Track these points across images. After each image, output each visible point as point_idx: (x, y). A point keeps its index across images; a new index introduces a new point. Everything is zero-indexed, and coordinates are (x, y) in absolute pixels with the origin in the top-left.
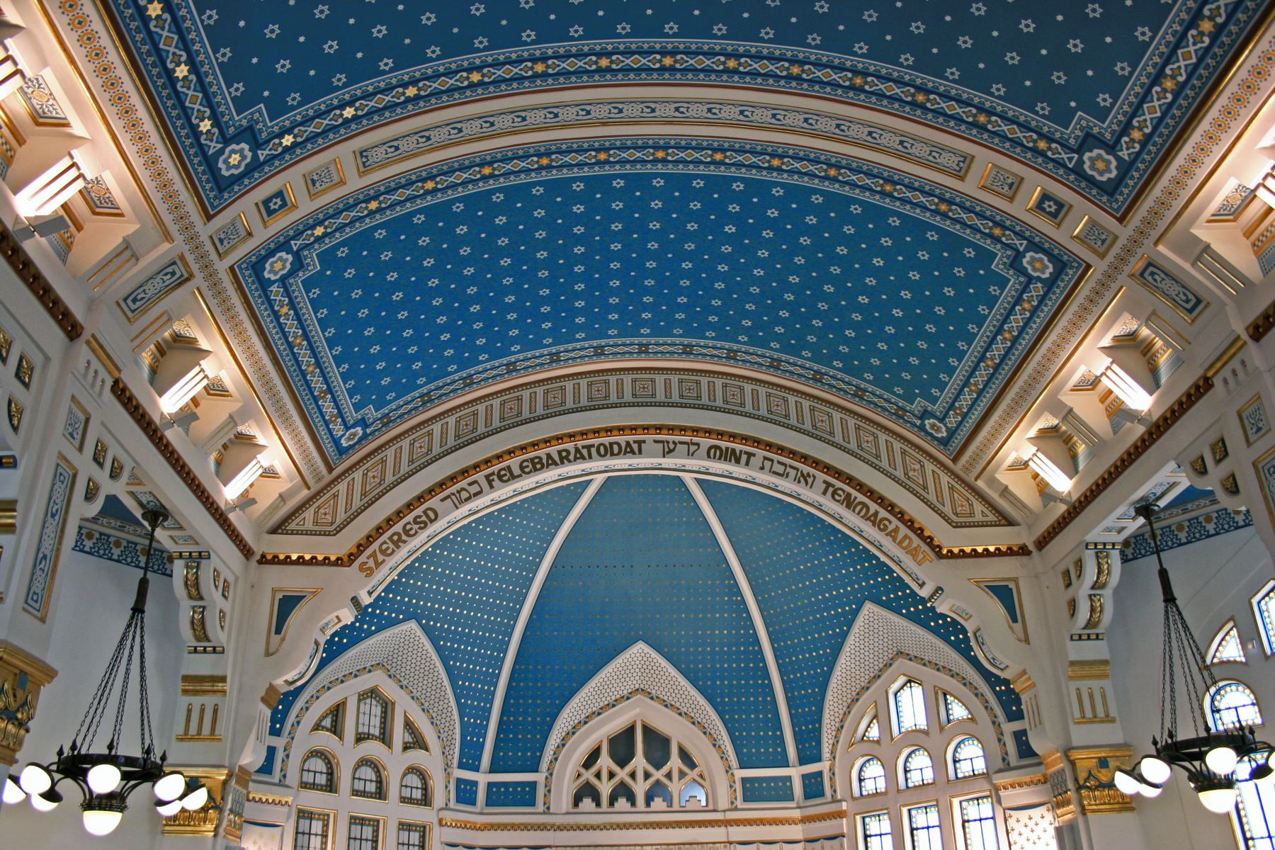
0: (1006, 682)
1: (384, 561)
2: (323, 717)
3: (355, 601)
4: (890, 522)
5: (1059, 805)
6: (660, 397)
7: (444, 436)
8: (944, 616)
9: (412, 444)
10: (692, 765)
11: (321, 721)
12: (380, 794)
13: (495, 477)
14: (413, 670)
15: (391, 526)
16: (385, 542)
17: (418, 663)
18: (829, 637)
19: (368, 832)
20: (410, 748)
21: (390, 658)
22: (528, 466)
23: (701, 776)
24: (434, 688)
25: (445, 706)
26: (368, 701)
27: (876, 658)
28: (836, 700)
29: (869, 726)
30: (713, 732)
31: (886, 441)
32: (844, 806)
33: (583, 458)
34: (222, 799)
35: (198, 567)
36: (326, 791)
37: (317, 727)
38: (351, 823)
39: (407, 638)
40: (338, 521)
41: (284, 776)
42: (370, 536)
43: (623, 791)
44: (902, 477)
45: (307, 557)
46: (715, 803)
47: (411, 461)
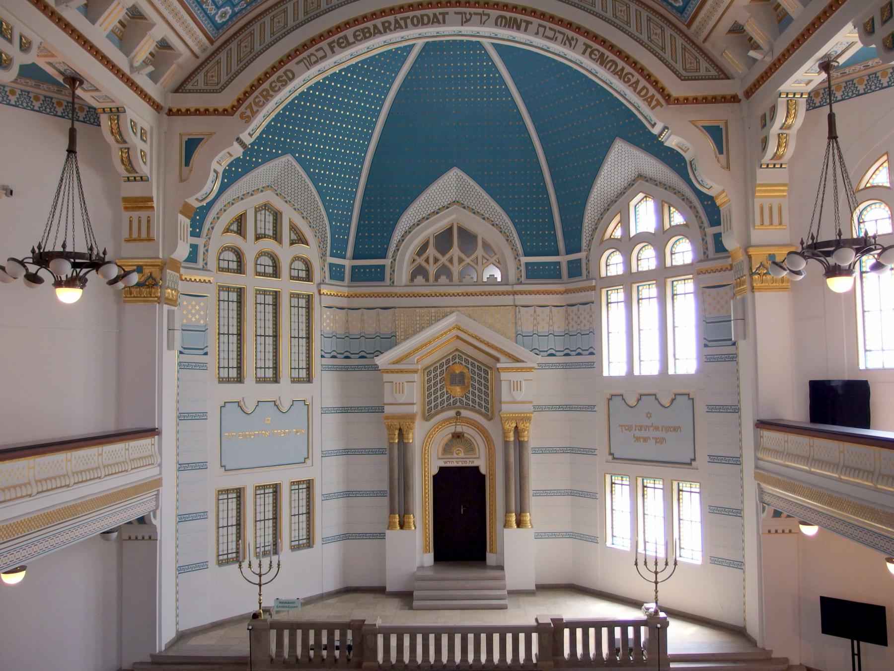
0: (711, 198)
1: (258, 111)
4: (633, 76)
9: (272, 20)
11: (229, 226)
13: (335, 44)
16: (257, 97)
17: (296, 185)
21: (276, 182)
22: (360, 35)
30: (506, 231)
31: (636, 10)
35: (118, 119)
36: (237, 273)
37: (227, 230)
38: (256, 294)
40: (223, 81)
41: (206, 264)
43: (444, 271)
47: (273, 34)
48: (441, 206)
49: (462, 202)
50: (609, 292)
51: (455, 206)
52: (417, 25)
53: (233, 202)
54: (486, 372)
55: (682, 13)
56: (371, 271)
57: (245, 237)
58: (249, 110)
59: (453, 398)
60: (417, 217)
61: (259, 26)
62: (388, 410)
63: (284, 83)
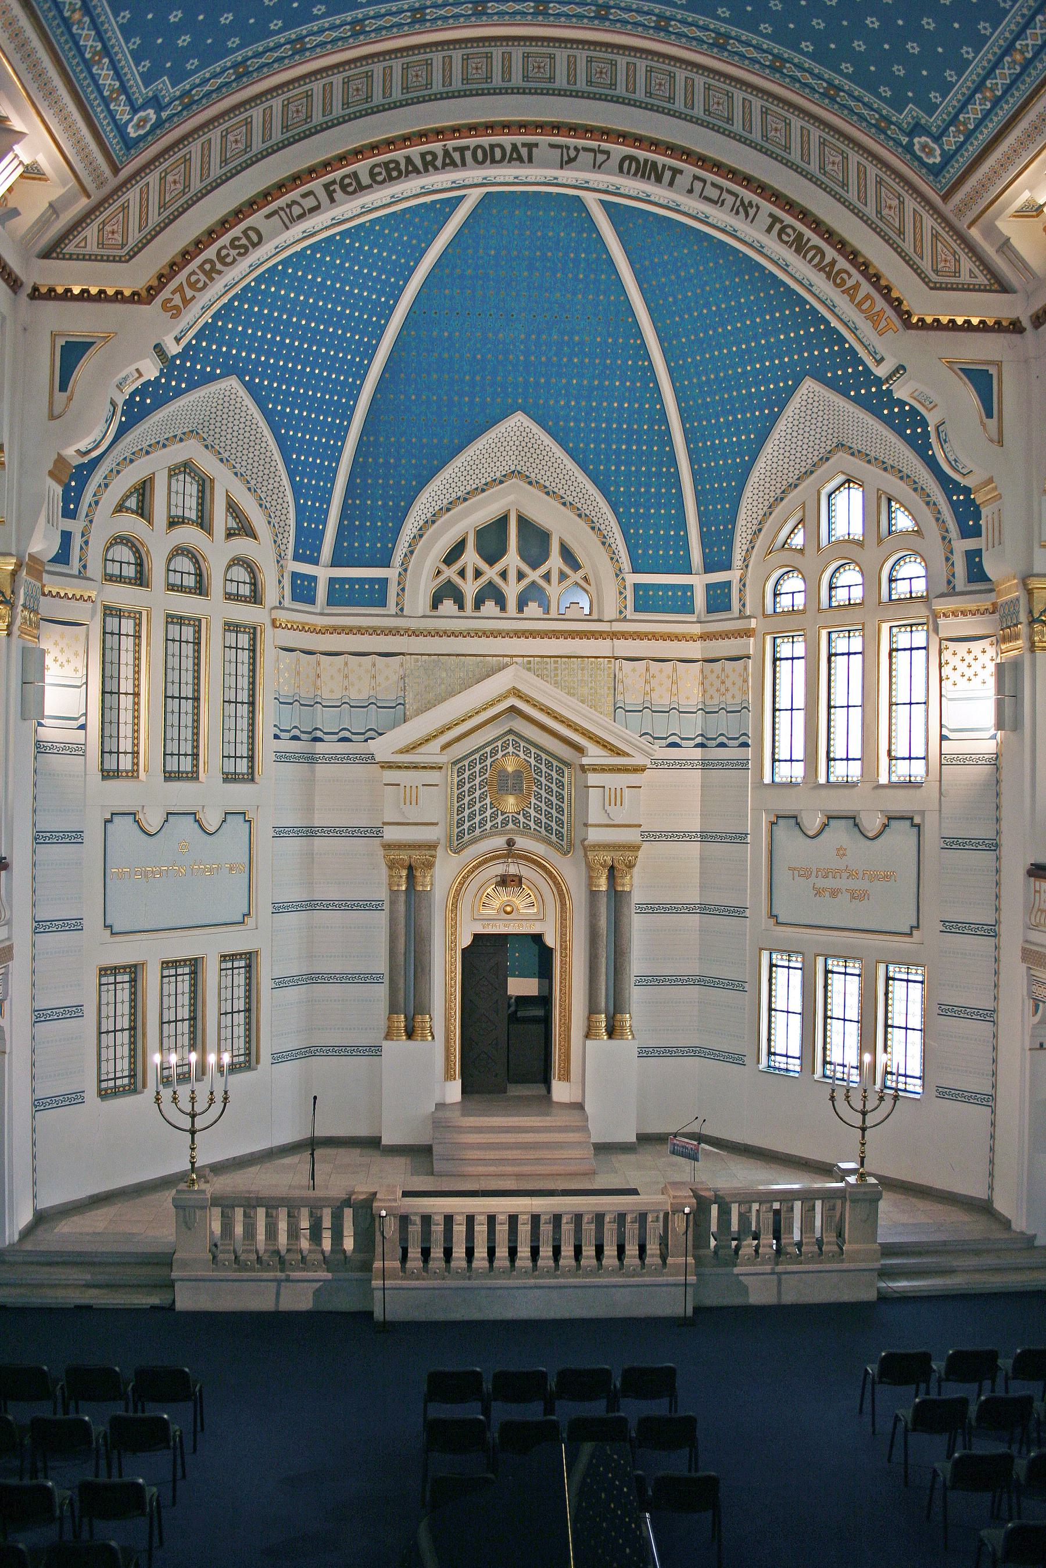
0: (967, 491)
1: (194, 297)
2: (126, 497)
3: (159, 350)
4: (850, 276)
5: (1005, 639)
6: (561, 82)
7: (267, 125)
8: (901, 403)
10: (576, 566)
11: (124, 501)
12: (201, 588)
13: (337, 187)
14: (235, 440)
15: (202, 251)
16: (194, 273)
17: (241, 431)
18: (755, 420)
19: (188, 633)
20: (235, 535)
22: (380, 174)
23: (585, 579)
24: (262, 462)
25: (276, 485)
26: (181, 477)
27: (810, 450)
28: (755, 497)
29: (792, 532)
30: (603, 527)
32: (753, 623)
33: (453, 164)
34: (13, 592)
36: (135, 584)
37: (120, 508)
38: (167, 622)
39: (227, 399)
40: (131, 242)
41: (85, 567)
42: (174, 264)
43: (492, 593)
44: (873, 216)
45: (94, 291)
46: (601, 611)
47: (224, 162)
48: (489, 479)
49: (527, 473)
50: (778, 641)
51: (514, 480)
52: (484, 162)
53: (133, 457)
54: (561, 773)
55: (936, 175)
56: (352, 588)
57: (150, 521)
58: (178, 295)
59: (502, 814)
60: (447, 496)
61: (199, 146)
62: (391, 834)
63: (242, 251)
